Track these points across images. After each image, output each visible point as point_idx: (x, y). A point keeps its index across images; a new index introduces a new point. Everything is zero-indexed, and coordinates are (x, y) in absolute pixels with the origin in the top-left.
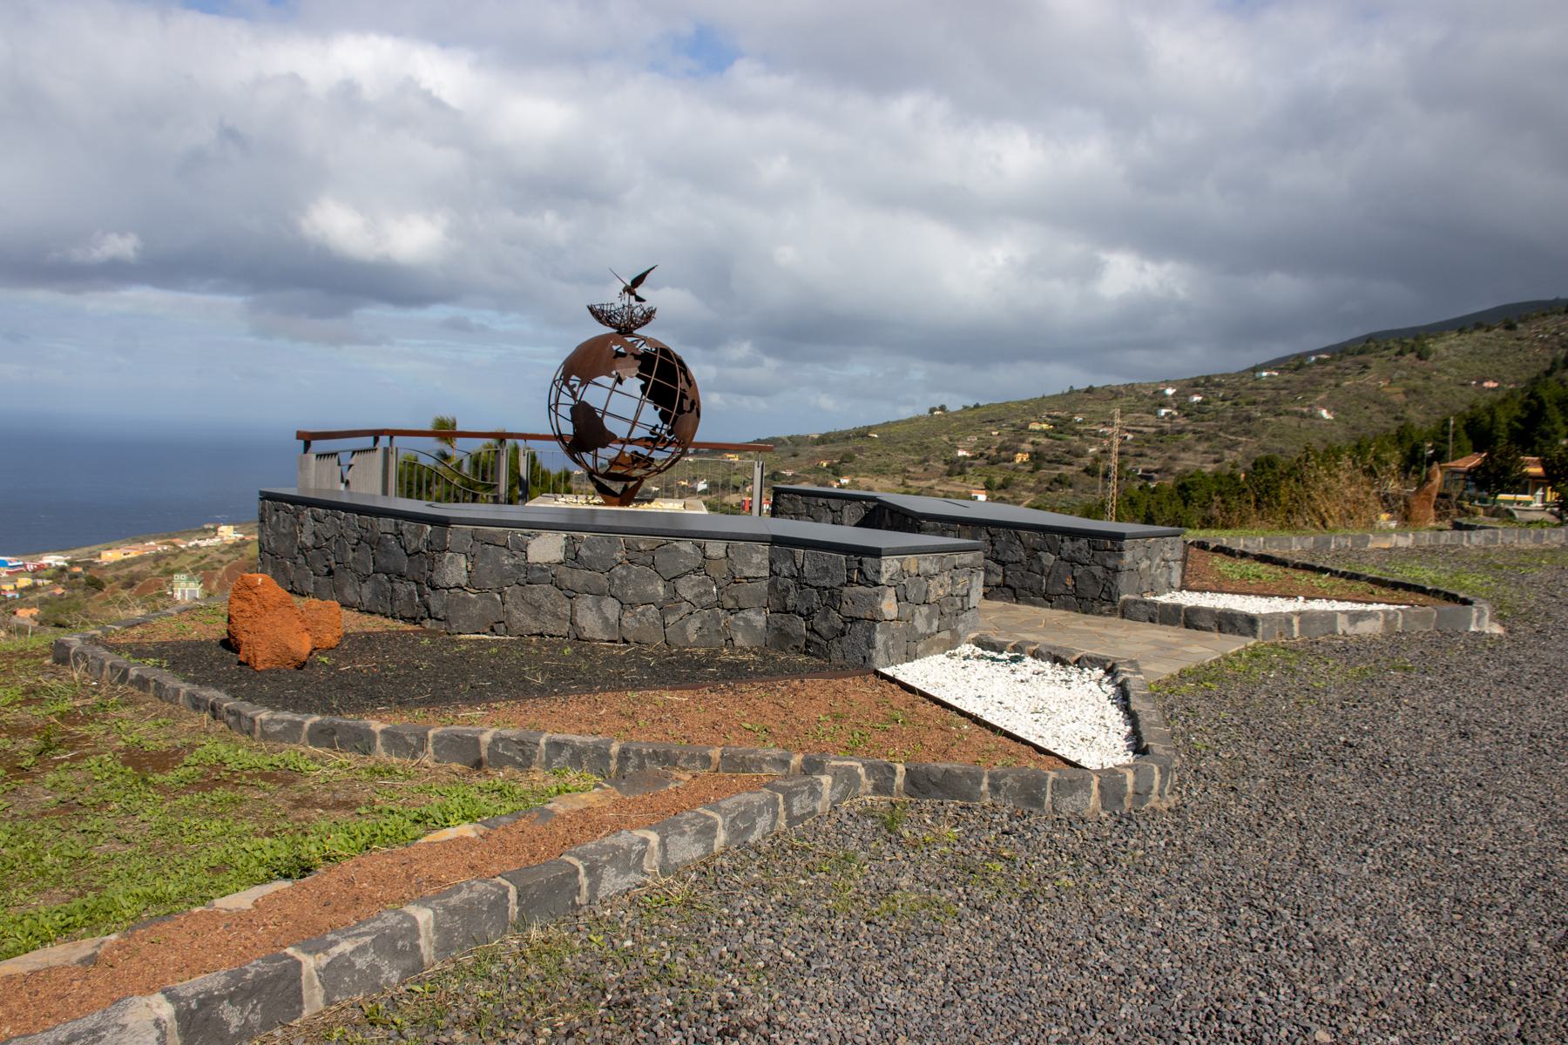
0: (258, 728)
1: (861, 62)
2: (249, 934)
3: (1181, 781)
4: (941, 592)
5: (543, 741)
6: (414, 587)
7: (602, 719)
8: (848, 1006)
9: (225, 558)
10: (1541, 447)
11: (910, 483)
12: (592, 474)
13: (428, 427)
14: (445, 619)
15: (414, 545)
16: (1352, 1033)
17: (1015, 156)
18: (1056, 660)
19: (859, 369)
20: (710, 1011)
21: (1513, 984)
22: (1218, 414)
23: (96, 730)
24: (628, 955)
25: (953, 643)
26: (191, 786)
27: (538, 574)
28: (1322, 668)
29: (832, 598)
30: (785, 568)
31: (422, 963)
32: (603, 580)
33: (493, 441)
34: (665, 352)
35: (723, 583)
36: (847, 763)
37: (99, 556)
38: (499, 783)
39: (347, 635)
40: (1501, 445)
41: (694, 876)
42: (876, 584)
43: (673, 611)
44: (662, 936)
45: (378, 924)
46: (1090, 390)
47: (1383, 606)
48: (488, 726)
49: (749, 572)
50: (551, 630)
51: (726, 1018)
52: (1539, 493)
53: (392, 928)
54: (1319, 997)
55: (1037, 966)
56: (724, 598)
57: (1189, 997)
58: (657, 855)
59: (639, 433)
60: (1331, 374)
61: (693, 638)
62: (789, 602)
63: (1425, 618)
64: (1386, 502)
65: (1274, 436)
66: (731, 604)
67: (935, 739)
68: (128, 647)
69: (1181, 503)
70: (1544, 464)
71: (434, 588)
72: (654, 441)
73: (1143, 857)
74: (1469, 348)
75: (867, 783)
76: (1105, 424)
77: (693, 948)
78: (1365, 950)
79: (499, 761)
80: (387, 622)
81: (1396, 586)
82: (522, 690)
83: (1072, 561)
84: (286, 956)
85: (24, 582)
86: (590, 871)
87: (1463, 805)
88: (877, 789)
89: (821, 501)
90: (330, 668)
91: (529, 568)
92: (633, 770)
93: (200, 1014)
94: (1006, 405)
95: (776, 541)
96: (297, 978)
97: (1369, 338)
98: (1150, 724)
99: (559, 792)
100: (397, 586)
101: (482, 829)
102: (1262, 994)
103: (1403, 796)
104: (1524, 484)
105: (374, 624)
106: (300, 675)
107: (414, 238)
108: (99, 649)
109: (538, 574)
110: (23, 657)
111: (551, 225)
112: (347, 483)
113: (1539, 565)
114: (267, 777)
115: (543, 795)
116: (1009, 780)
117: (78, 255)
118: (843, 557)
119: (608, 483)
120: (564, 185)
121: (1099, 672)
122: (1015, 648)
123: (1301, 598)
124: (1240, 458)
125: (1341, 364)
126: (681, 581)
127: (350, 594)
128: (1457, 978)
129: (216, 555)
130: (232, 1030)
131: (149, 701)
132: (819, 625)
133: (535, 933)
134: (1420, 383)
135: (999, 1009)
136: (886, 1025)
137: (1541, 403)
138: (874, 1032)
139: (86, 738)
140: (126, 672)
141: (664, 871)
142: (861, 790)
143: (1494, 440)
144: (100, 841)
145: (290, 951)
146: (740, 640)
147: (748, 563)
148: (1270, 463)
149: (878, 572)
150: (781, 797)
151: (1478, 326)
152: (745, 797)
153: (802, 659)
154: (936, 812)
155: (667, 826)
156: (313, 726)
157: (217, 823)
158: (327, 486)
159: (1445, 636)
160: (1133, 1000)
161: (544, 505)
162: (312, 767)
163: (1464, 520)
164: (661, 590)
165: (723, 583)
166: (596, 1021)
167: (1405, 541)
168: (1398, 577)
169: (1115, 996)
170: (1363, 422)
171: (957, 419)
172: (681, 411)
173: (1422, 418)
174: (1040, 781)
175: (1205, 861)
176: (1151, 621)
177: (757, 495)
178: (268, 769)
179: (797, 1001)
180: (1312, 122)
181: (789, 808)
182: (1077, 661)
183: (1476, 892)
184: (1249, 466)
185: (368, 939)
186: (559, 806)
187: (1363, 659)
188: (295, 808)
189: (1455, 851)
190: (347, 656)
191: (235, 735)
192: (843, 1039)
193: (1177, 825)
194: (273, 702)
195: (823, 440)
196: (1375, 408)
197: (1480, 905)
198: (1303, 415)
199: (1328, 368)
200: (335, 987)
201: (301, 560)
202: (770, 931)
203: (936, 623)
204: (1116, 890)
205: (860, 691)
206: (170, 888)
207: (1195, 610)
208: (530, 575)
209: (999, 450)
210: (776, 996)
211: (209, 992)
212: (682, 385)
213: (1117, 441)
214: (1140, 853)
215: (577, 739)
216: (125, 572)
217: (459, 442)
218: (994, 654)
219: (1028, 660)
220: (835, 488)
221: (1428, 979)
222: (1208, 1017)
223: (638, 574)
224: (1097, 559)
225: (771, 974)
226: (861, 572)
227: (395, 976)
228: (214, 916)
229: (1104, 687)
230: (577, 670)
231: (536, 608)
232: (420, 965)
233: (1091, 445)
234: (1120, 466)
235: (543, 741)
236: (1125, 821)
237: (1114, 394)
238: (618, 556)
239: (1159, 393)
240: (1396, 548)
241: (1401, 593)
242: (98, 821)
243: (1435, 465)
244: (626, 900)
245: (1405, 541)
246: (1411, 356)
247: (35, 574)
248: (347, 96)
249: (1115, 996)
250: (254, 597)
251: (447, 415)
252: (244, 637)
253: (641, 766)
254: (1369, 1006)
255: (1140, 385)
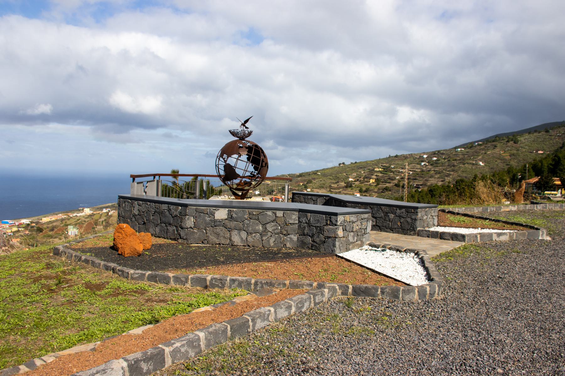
0: (130, 276)
1: (305, 39)
2: (144, 341)
3: (444, 290)
4: (357, 228)
5: (228, 279)
6: (175, 228)
7: (246, 272)
8: (343, 362)
9: (87, 220)
10: (560, 174)
11: (332, 190)
12: (231, 189)
13: (169, 172)
14: (186, 239)
15: (175, 214)
16: (510, 370)
17: (364, 72)
18: (398, 250)
19: (312, 149)
20: (298, 364)
21: (562, 354)
22: (443, 165)
23: (75, 277)
24: (268, 348)
25: (361, 245)
26: (110, 295)
27: (218, 223)
28: (489, 252)
29: (321, 230)
30: (304, 220)
31: (201, 350)
32: (241, 225)
33: (192, 177)
34: (256, 146)
35: (282, 225)
36: (332, 285)
37: (41, 220)
38: (214, 293)
39: (153, 245)
40: (545, 174)
41: (286, 322)
42: (336, 225)
43: (265, 235)
44: (278, 340)
45: (187, 337)
46: (396, 156)
47: (508, 231)
48: (209, 274)
49: (291, 222)
50: (223, 242)
51: (304, 366)
52: (560, 191)
53: (192, 338)
54: (498, 359)
55: (403, 349)
56: (283, 230)
57: (454, 358)
58: (273, 315)
59: (248, 174)
60: (483, 149)
61: (272, 244)
62: (305, 232)
63: (524, 235)
64: (506, 195)
65: (463, 172)
66: (285, 232)
67: (360, 277)
68: (79, 249)
69: (432, 195)
70: (561, 180)
71: (182, 228)
72: (252, 177)
73: (434, 315)
74: (533, 139)
75: (339, 292)
76: (402, 168)
77: (289, 345)
78: (512, 344)
79: (213, 286)
80: (165, 240)
81: (512, 224)
82: (217, 263)
83: (400, 217)
84: (159, 348)
85: (15, 229)
86: (253, 320)
87: (541, 297)
88: (343, 294)
89: (309, 197)
90: (150, 256)
91: (215, 221)
92: (261, 288)
93: (135, 366)
94: (366, 162)
95: (300, 211)
96: (164, 355)
97: (496, 136)
98: (433, 271)
99: (235, 296)
100: (169, 228)
101: (213, 308)
102: (478, 358)
103: (520, 294)
104: (555, 188)
105: (161, 241)
106: (140, 258)
107: (150, 105)
108: (69, 250)
109: (218, 223)
110: (41, 253)
111: (200, 100)
112: (146, 193)
113: (562, 216)
114: (135, 292)
115: (230, 297)
116: (387, 290)
117: (30, 112)
118: (324, 216)
119: (237, 192)
120: (204, 85)
121: (413, 254)
122: (383, 247)
123: (480, 229)
124: (451, 180)
125: (487, 146)
126: (268, 225)
127: (151, 230)
128: (543, 353)
129: (83, 219)
130: (144, 371)
131: (90, 267)
132: (316, 239)
133: (237, 341)
134: (515, 152)
135: (392, 363)
136: (356, 368)
137: (559, 158)
138: (352, 370)
139: (71, 280)
140: (81, 257)
141: (276, 320)
142: (337, 294)
143: (543, 172)
144: (84, 313)
145: (160, 346)
146: (288, 245)
147: (291, 219)
148: (462, 181)
149: (337, 221)
150: (312, 296)
151: (536, 131)
152: (300, 296)
153: (310, 251)
154: (363, 301)
155: (276, 304)
156: (149, 275)
157: (121, 307)
158: (140, 194)
159: (531, 241)
160: (436, 360)
161: (215, 199)
162: (150, 288)
163: (535, 201)
164: (261, 228)
165: (282, 225)
166: (262, 368)
167: (514, 208)
168: (512, 221)
169: (430, 359)
170: (495, 166)
171: (349, 167)
172: (262, 166)
173: (516, 164)
174: (398, 290)
175: (455, 316)
176: (428, 237)
177: (286, 196)
178: (135, 290)
179: (326, 361)
180: (471, 59)
181: (314, 300)
182: (405, 251)
183: (547, 325)
184: (454, 183)
185: (185, 342)
186: (237, 300)
187: (503, 249)
188: (147, 302)
189: (539, 312)
190: (154, 252)
191: (121, 278)
192: (343, 373)
193: (444, 304)
194: (132, 268)
195: (301, 175)
196: (499, 161)
197: (549, 330)
198: (473, 164)
199: (482, 147)
200: (175, 358)
201: (134, 219)
202: (313, 339)
203: (356, 238)
204: (426, 325)
205: (332, 262)
206: (111, 328)
207: (443, 233)
208: (215, 223)
209: (364, 178)
210: (319, 359)
211: (137, 358)
212: (262, 157)
213: (407, 174)
214: (433, 313)
215: (240, 278)
216: (51, 225)
217: (180, 178)
218: (376, 249)
219: (388, 250)
220: (305, 192)
221: (534, 353)
222: (461, 365)
223: (253, 223)
224: (409, 216)
225: (316, 353)
226: (330, 221)
227: (193, 354)
228: (130, 336)
229: (415, 259)
230: (233, 256)
231: (218, 235)
232: (201, 351)
233: (397, 175)
234: (408, 183)
235: (228, 279)
236: (427, 303)
237: (405, 157)
238: (246, 216)
239: (421, 157)
240: (511, 211)
241: (514, 226)
242: (82, 307)
243: (523, 181)
244: (264, 330)
245: (514, 208)
246: (512, 142)
247: (18, 226)
248: (125, 56)
249: (430, 359)
250: (123, 232)
251: (175, 169)
252: (120, 246)
253: (262, 287)
254: (514, 361)
255: (415, 154)
